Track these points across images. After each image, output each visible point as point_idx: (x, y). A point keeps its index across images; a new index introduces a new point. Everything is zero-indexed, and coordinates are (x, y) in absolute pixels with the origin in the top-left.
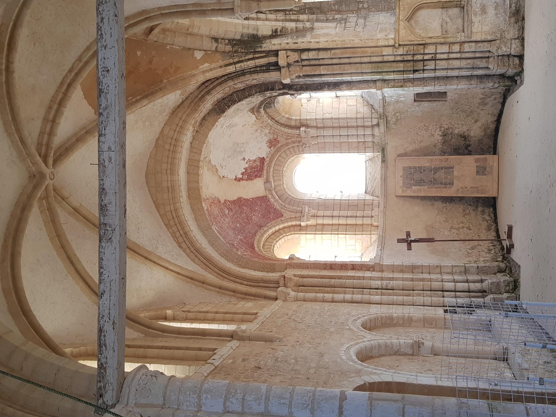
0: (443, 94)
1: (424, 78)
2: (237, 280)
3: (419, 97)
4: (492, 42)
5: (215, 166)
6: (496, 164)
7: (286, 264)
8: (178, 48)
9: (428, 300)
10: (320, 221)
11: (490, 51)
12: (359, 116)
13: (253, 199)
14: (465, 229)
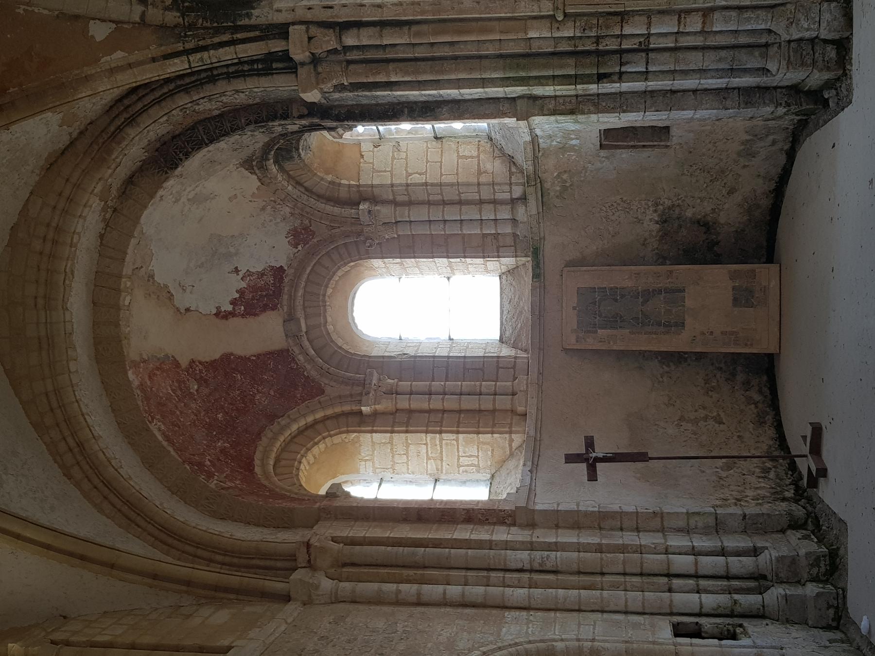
0: (666, 130)
1: (621, 94)
2: (200, 552)
3: (611, 138)
4: (775, 10)
5: (166, 286)
6: (774, 283)
7: (319, 509)
8: (46, 12)
9: (635, 598)
10: (403, 403)
11: (770, 31)
12: (483, 179)
13: (258, 356)
14: (711, 422)
